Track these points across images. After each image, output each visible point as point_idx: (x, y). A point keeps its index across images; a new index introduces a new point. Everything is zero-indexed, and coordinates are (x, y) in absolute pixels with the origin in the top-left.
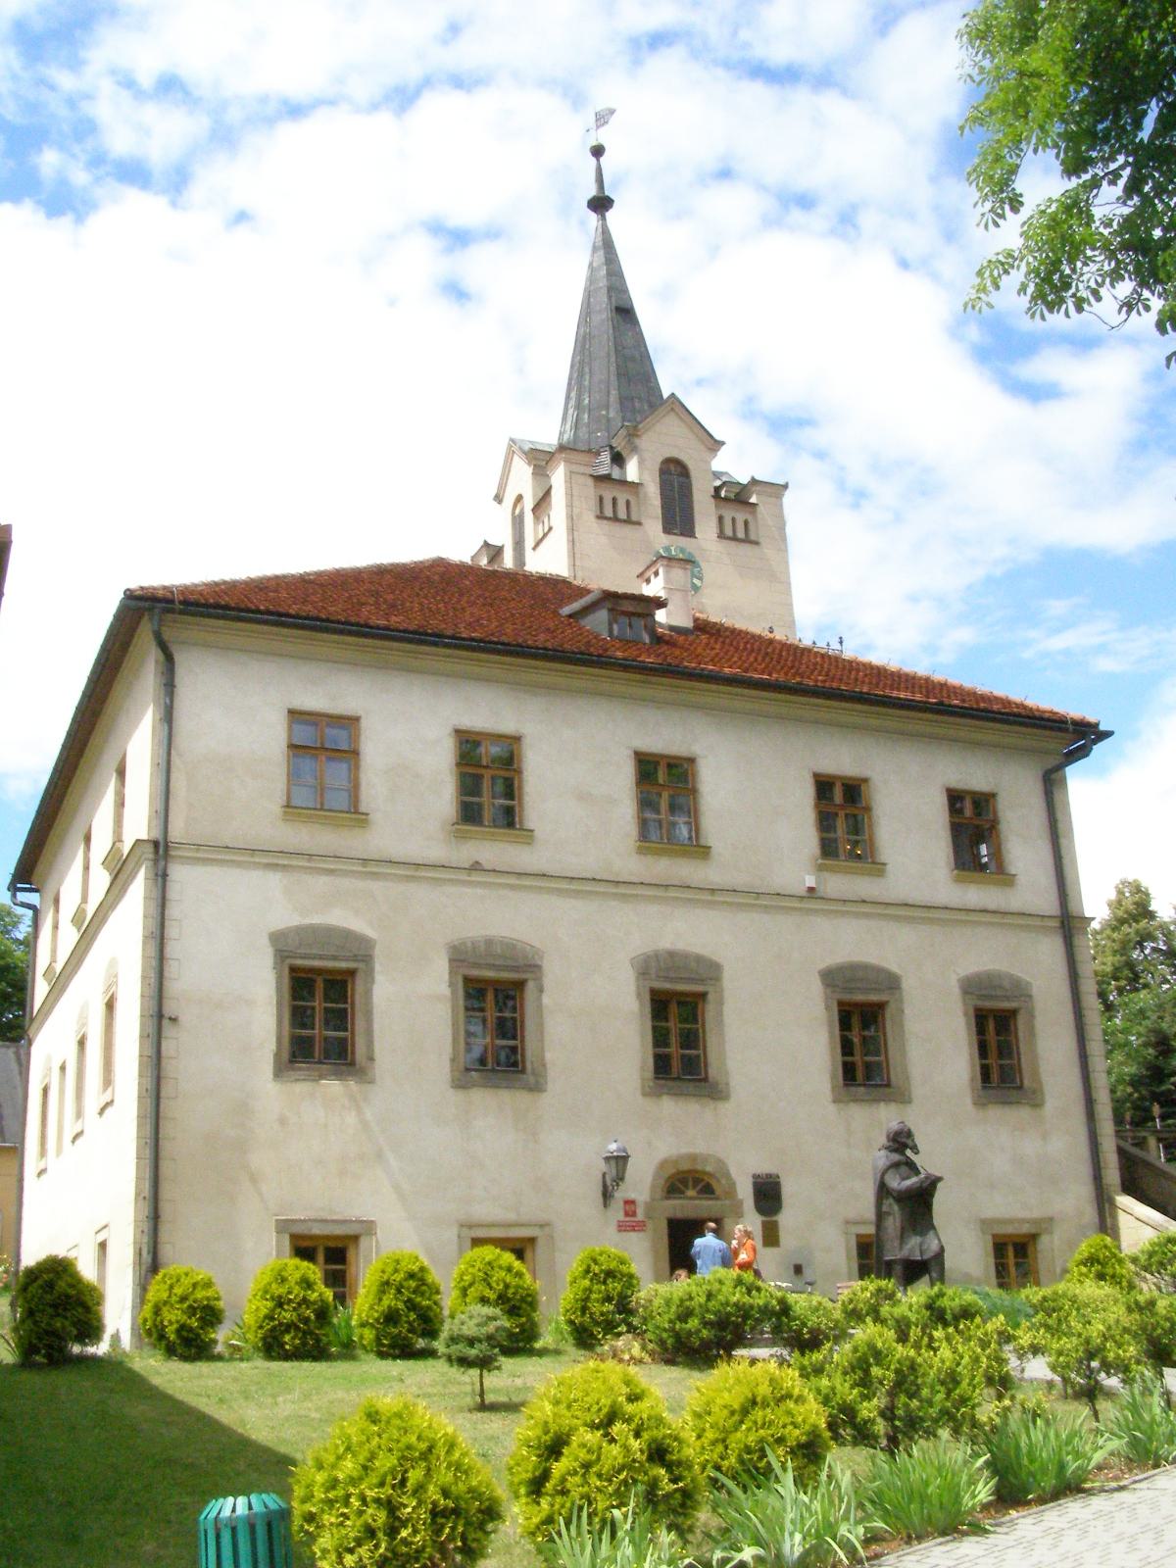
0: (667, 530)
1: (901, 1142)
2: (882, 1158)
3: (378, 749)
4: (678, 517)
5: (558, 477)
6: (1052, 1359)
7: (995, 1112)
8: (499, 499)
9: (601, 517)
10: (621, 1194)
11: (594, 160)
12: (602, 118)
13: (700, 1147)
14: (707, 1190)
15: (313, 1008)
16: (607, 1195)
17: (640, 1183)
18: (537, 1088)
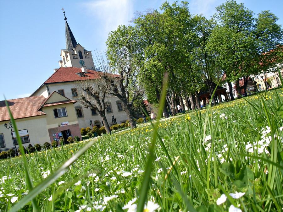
0: (80, 59)
1: (113, 116)
2: (112, 118)
3: (65, 92)
4: (81, 57)
5: (68, 54)
6: (257, 84)
7: (120, 112)
8: (61, 56)
9: (74, 59)
10: (92, 124)
11: (66, 18)
12: (63, 9)
13: (97, 119)
14: (98, 123)
15: (128, 128)
16: (91, 124)
17: (93, 123)
18: (84, 117)
